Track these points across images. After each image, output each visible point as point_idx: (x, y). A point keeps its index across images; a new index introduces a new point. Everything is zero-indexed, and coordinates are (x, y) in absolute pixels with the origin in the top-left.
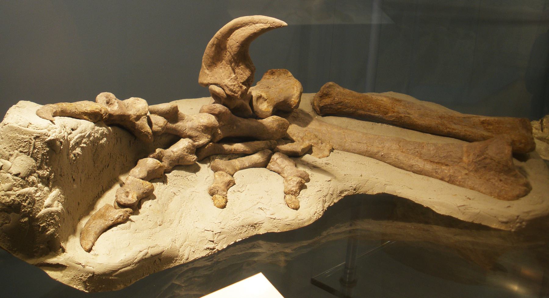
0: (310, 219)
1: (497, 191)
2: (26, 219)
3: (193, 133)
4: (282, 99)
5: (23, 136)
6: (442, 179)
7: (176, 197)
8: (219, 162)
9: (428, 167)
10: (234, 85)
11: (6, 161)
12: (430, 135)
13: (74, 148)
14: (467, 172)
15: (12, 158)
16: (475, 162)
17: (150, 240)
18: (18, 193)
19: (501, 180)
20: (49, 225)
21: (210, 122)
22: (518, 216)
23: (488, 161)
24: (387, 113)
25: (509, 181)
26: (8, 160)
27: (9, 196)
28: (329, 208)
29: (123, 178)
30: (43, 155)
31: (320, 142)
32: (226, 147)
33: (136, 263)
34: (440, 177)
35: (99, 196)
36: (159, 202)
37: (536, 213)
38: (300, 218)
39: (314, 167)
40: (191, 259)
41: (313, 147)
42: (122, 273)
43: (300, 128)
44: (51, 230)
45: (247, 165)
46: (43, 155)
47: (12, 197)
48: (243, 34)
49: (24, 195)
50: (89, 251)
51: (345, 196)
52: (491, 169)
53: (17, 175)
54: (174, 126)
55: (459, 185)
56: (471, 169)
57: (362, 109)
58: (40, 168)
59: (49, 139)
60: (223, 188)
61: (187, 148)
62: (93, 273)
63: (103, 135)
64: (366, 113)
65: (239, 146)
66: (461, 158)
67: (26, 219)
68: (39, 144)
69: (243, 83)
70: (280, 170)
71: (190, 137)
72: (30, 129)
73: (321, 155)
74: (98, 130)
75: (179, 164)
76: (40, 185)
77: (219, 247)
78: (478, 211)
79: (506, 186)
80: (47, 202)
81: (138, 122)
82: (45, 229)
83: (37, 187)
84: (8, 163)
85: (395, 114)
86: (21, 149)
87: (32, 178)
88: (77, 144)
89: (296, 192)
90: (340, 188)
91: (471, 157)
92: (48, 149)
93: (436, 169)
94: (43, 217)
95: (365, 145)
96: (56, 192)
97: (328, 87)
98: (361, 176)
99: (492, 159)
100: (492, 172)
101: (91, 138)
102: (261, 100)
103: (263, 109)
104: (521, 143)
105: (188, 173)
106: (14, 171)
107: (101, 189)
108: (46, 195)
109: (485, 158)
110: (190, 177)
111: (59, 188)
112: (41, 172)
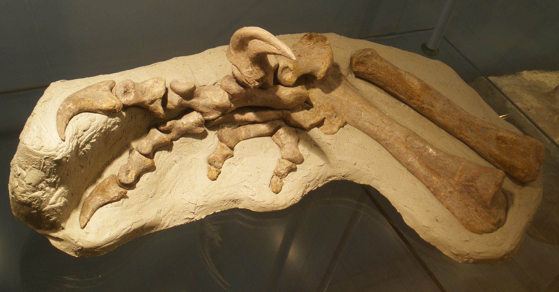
0: (286, 204)
1: (468, 219)
2: (35, 211)
3: (205, 110)
4: (308, 71)
5: (35, 157)
6: (428, 187)
7: (176, 165)
8: (226, 131)
9: (422, 171)
10: (250, 78)
11: (23, 171)
12: (444, 132)
13: (84, 146)
14: (452, 190)
15: (27, 170)
16: (464, 185)
17: (137, 215)
18: (30, 196)
19: (476, 211)
20: (52, 215)
21: (222, 103)
22: (468, 254)
23: (473, 190)
24: (411, 99)
25: (483, 215)
26: (25, 170)
27: (23, 197)
28: (311, 192)
29: (134, 144)
30: (51, 169)
31: (334, 115)
32: (238, 117)
33: (118, 239)
34: (427, 185)
35: (109, 163)
36: (158, 173)
37: (486, 255)
38: (275, 203)
39: (315, 146)
40: (171, 226)
41: (326, 119)
42: (104, 248)
43: (322, 94)
44: (54, 218)
45: (252, 136)
46: (51, 169)
47: (25, 199)
48: (260, 47)
49: (34, 198)
50: (83, 228)
51: (331, 181)
52: (473, 197)
53: (30, 184)
54: (188, 102)
55: (439, 200)
56: (457, 189)
57: (391, 87)
58: (48, 177)
59: (56, 159)
60: (220, 159)
61: (196, 123)
62: (82, 248)
63: (114, 124)
64: (393, 91)
65: (250, 116)
66: (453, 175)
67: (35, 211)
68: (48, 162)
69: (256, 80)
70: (281, 145)
71: (202, 113)
72: (41, 152)
73: (328, 131)
74: (110, 122)
75: (187, 133)
76: (48, 188)
77: (197, 218)
78: (437, 236)
79: (478, 218)
80: (52, 200)
81: (152, 105)
82: (49, 218)
83: (45, 190)
84: (24, 173)
85: (419, 103)
86: (33, 166)
87: (42, 185)
88: (87, 142)
89: (283, 175)
90: (329, 174)
91: (463, 178)
92: (55, 165)
93: (430, 172)
94: (48, 211)
95: (376, 128)
96: (61, 190)
97: (365, 57)
98: (355, 164)
99: (477, 190)
100: (473, 200)
101: (102, 131)
102: (287, 70)
103: (287, 79)
104: (523, 172)
105: (194, 140)
106: (28, 180)
107: (111, 157)
108: (52, 195)
109: (472, 186)
110: (196, 143)
111: (64, 186)
112: (48, 180)
